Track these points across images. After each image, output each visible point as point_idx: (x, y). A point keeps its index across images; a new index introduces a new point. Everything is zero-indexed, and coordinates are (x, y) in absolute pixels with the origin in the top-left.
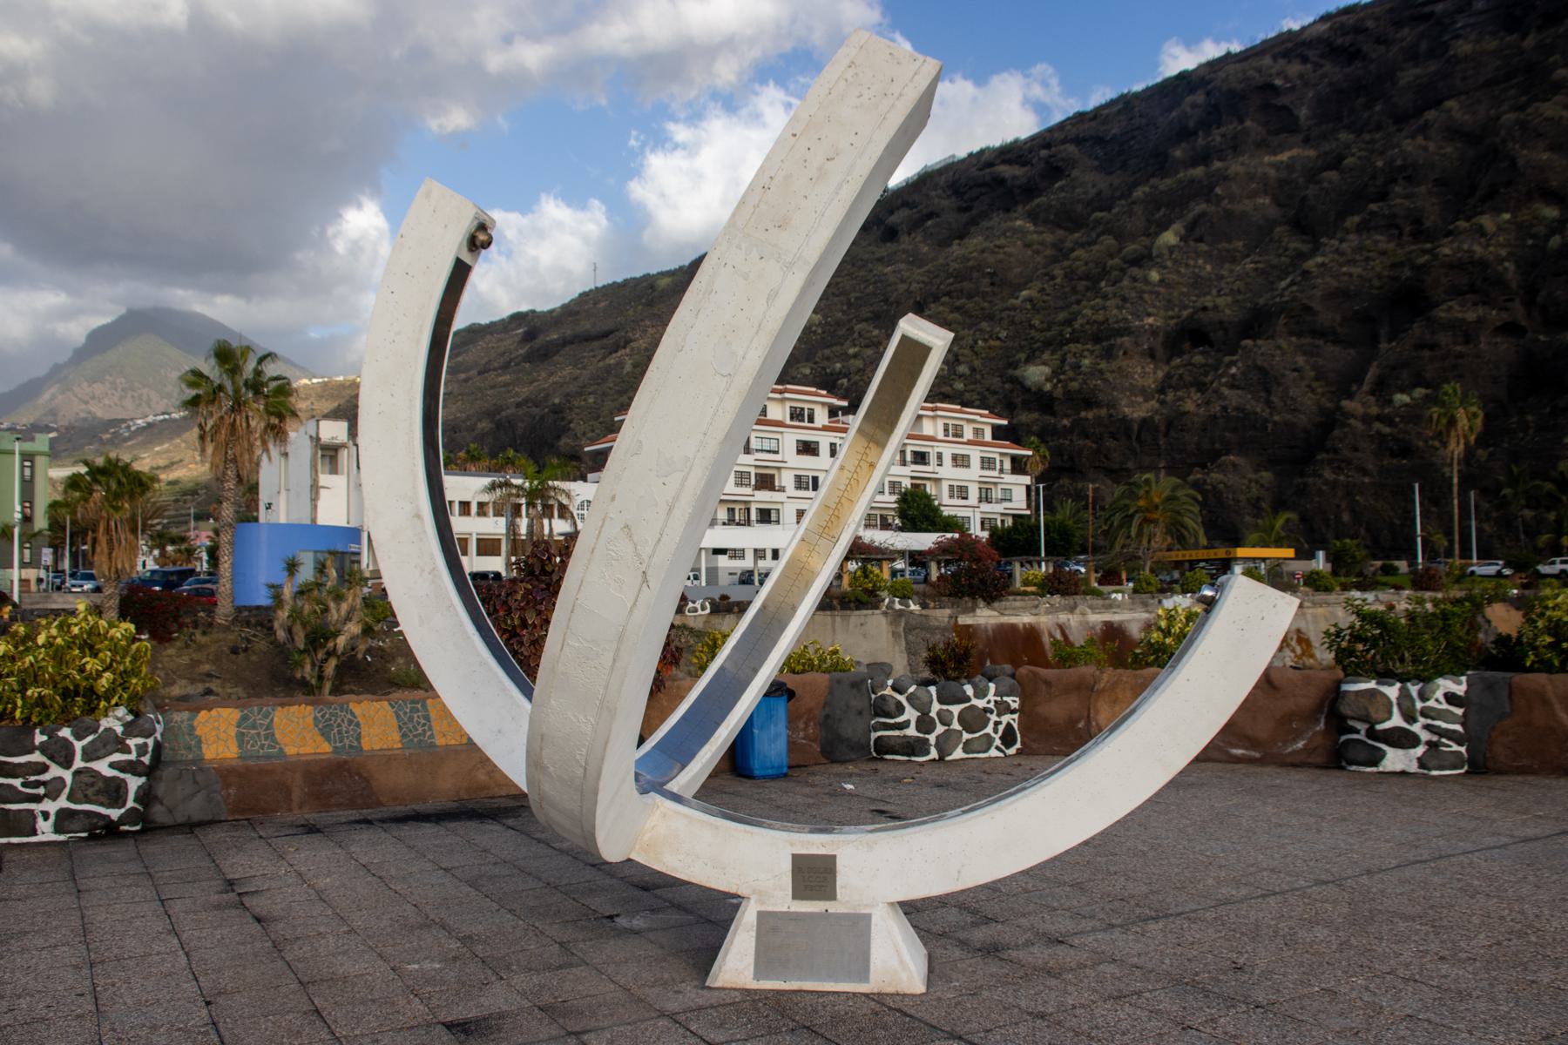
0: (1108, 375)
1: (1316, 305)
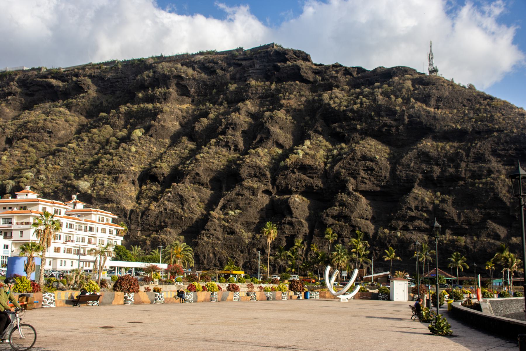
0: (117, 190)
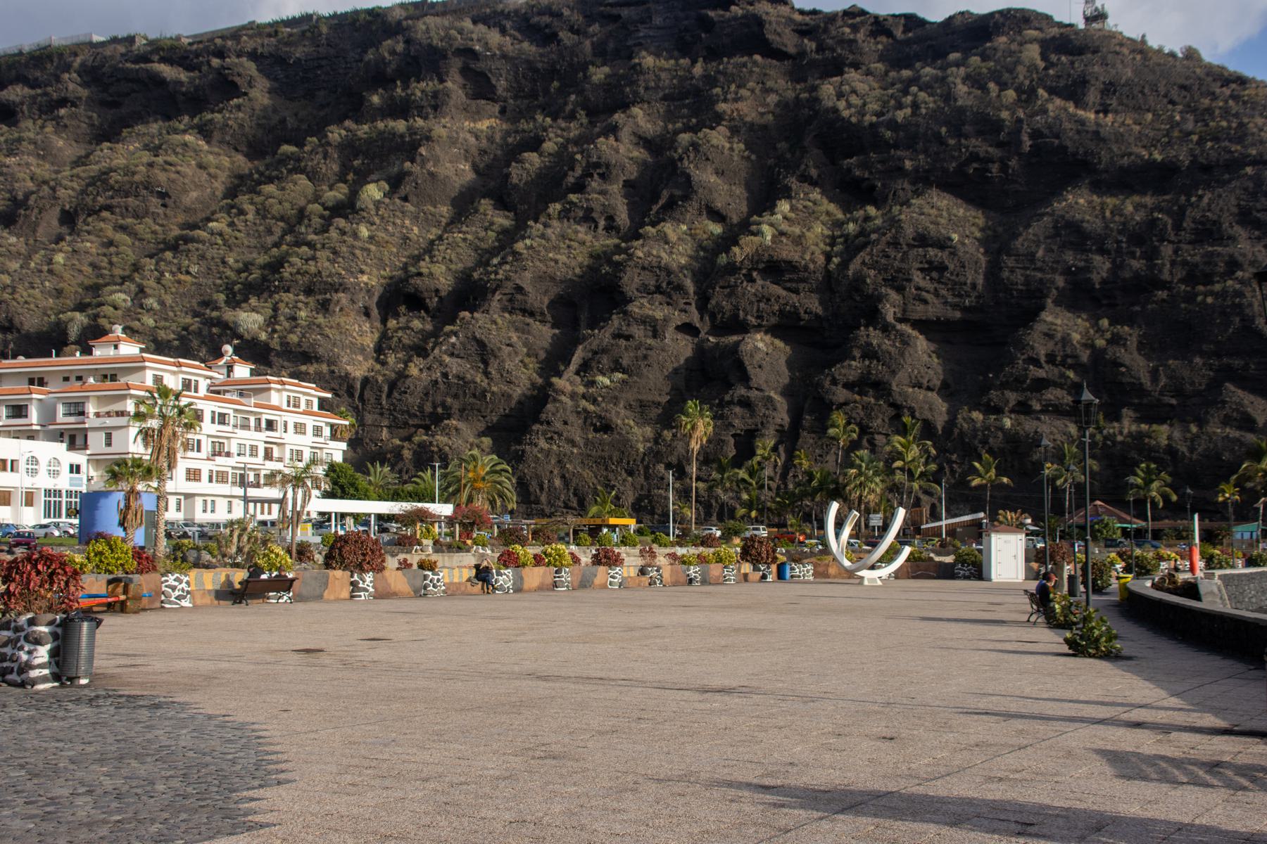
0: (328, 331)
1: (528, 287)
